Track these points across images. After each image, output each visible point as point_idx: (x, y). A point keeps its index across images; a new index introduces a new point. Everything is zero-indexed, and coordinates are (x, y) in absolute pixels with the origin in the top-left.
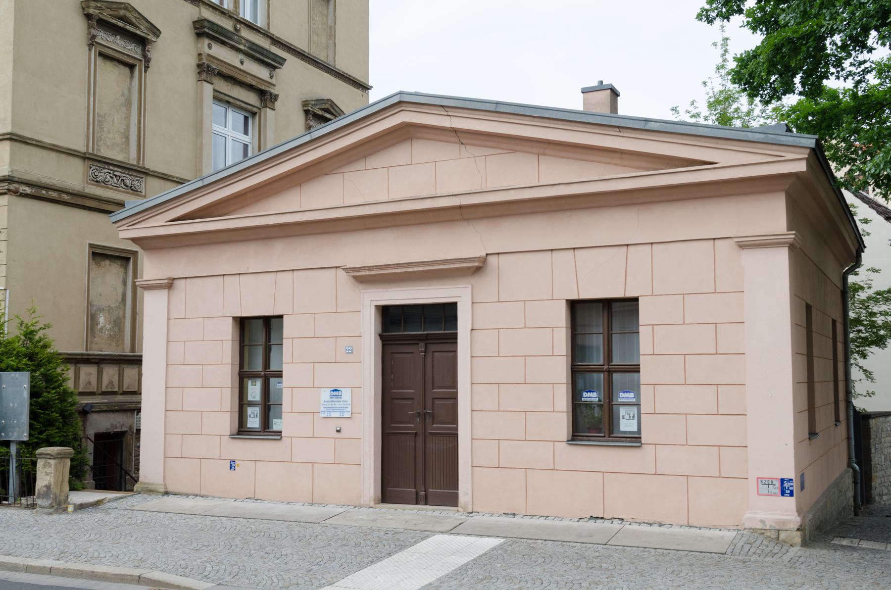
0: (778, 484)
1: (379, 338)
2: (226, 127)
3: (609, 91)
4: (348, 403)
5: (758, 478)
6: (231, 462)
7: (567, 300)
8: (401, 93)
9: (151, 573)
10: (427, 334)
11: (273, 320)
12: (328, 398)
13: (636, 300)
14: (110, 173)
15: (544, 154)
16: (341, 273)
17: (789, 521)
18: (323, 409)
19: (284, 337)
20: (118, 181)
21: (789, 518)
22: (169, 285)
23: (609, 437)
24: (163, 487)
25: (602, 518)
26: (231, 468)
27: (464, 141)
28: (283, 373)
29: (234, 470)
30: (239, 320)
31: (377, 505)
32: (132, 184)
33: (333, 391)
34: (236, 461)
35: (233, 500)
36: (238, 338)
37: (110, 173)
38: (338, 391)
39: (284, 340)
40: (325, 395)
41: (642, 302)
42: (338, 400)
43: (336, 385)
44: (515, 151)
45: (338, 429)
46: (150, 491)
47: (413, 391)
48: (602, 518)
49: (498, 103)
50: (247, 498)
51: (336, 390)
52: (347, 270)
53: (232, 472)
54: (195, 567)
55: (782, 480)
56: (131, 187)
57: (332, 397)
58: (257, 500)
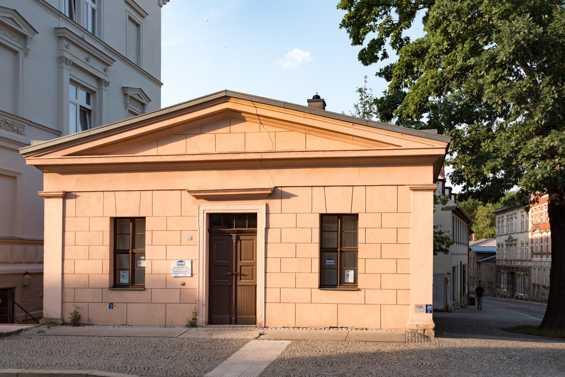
0: (425, 307)
1: (208, 232)
2: (76, 99)
3: (323, 102)
4: (189, 269)
5: (415, 305)
6: (110, 304)
7: (319, 214)
8: (226, 91)
9: (94, 372)
10: (238, 230)
11: (137, 220)
12: (176, 266)
13: (144, 218)
14: (3, 121)
15: (310, 134)
16: (185, 193)
17: (430, 325)
18: (173, 272)
19: (146, 230)
20: (9, 126)
21: (430, 323)
22: (66, 196)
23: (132, 286)
24: (61, 320)
25: (336, 327)
26: (110, 308)
27: (262, 122)
28: (146, 251)
29: (112, 308)
30: (114, 218)
31: (207, 326)
32: (18, 130)
33: (179, 262)
34: (114, 303)
35: (112, 326)
36: (113, 230)
37: (3, 121)
38: (183, 261)
39: (146, 232)
40: (174, 264)
41: (147, 219)
42: (182, 267)
43: (180, 259)
44: (293, 131)
45: (183, 283)
46: (84, 325)
47: (227, 261)
48: (336, 327)
49: (285, 103)
50: (121, 325)
51: (181, 261)
52: (189, 192)
53: (111, 310)
54: (119, 367)
55: (427, 305)
56: (18, 131)
57: (178, 265)
58: (129, 326)
